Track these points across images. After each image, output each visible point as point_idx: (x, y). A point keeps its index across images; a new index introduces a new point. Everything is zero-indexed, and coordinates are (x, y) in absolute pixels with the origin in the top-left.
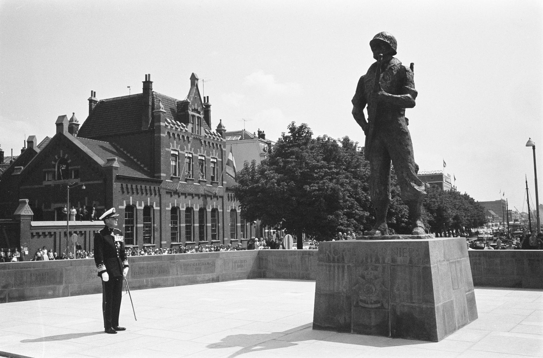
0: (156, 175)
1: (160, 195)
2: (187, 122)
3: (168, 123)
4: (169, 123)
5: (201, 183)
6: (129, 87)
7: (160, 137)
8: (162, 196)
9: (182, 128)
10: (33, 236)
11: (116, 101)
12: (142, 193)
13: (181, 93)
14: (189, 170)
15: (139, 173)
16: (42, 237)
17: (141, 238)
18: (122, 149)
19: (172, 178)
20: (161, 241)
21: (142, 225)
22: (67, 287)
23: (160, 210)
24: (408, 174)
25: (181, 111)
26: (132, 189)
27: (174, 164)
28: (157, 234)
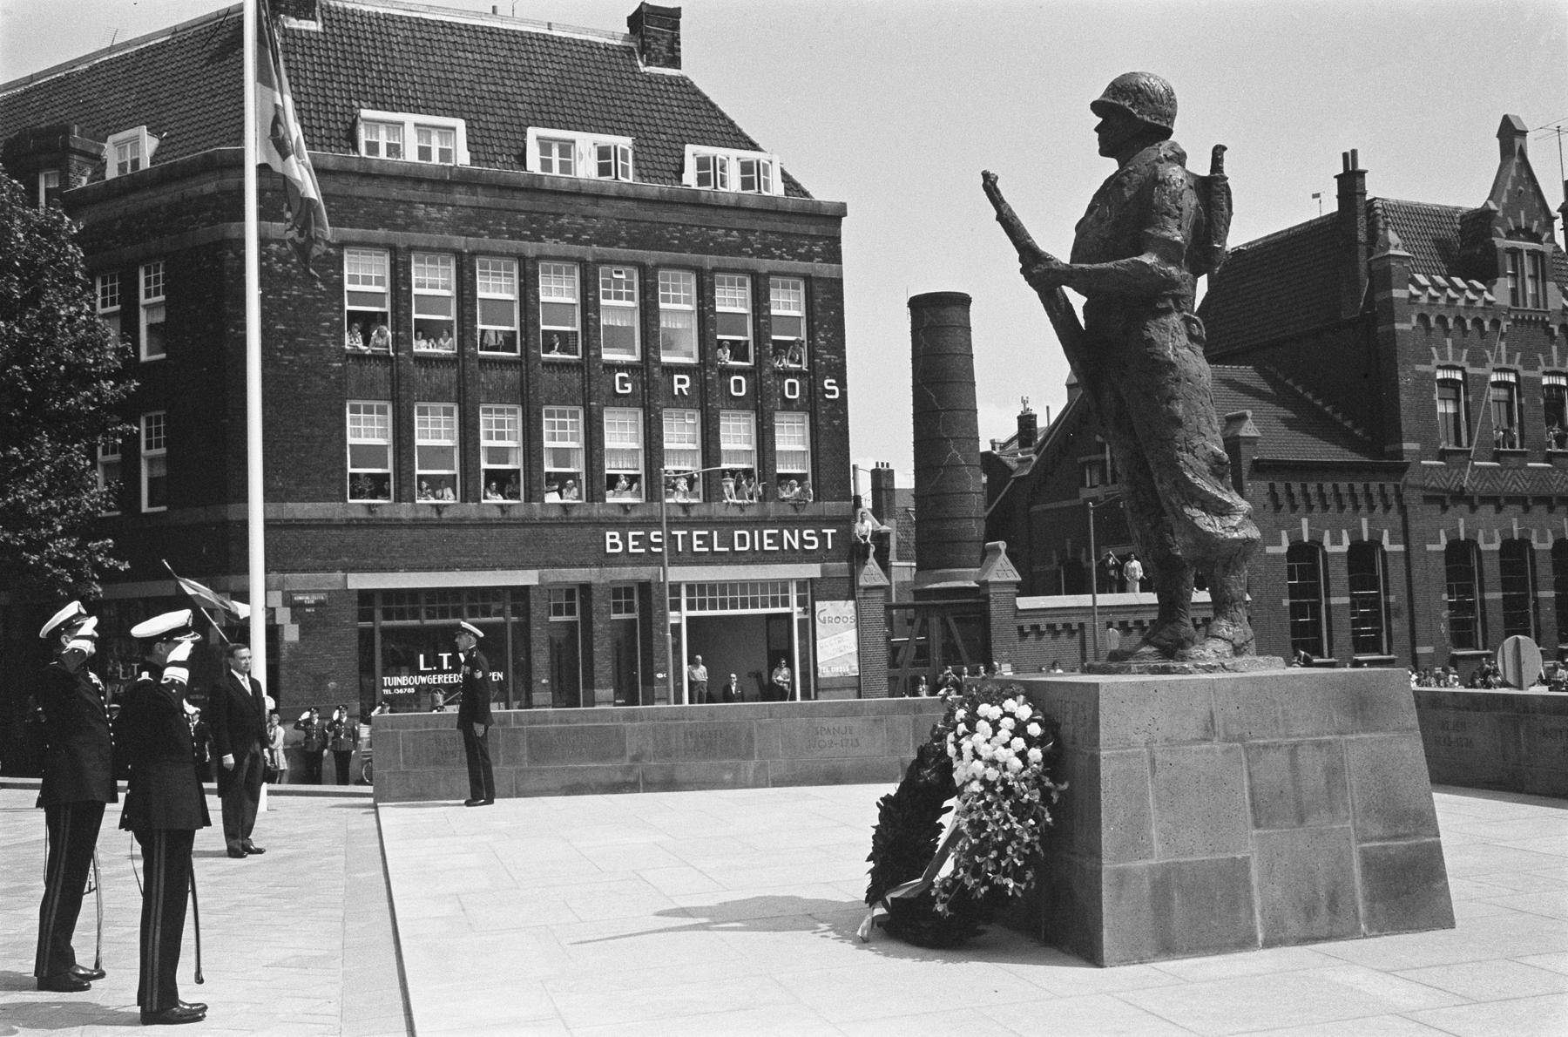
0: (1388, 448)
1: (1403, 509)
2: (1489, 275)
3: (1421, 287)
4: (1423, 288)
5: (1556, 460)
6: (1316, 196)
7: (1393, 333)
8: (1410, 510)
9: (1472, 296)
10: (1023, 634)
11: (1276, 243)
12: (1341, 507)
13: (1468, 186)
14: (1510, 421)
15: (1333, 448)
16: (1064, 635)
17: (1344, 637)
18: (1290, 382)
19: (1443, 455)
20: (1414, 644)
21: (1347, 600)
22: (763, 767)
23: (1407, 554)
24: (1175, 483)
25: (1468, 244)
26: (1306, 496)
27: (1451, 409)
28: (1399, 626)
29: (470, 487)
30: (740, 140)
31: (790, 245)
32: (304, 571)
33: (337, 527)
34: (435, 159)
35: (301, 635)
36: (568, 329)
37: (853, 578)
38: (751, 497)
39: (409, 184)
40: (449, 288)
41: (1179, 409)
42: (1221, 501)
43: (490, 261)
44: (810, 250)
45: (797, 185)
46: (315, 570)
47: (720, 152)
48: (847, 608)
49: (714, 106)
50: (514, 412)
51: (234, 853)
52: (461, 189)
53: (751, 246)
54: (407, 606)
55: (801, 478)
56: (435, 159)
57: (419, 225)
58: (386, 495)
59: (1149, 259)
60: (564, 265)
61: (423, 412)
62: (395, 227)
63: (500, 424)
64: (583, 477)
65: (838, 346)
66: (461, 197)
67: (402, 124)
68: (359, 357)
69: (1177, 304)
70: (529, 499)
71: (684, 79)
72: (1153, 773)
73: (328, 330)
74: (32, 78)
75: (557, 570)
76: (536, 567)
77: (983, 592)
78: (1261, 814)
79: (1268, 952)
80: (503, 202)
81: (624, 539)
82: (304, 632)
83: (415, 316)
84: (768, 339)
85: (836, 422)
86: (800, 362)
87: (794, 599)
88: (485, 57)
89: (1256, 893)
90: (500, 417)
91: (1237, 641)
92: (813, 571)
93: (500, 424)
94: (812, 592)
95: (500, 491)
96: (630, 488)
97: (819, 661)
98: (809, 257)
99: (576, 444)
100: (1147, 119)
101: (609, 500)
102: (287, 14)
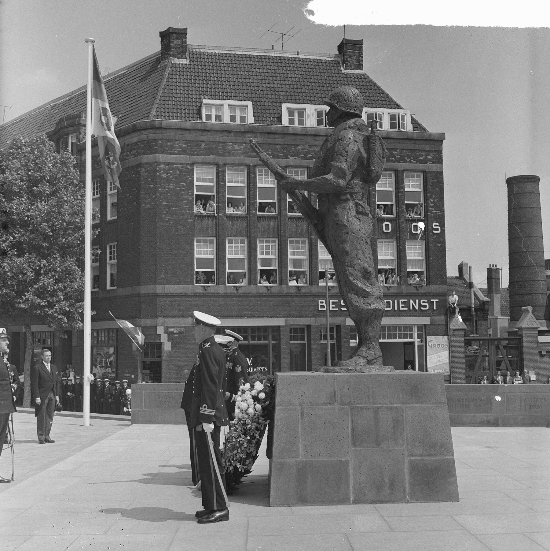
10: (542, 355)
29: (252, 278)
30: (390, 103)
31: (414, 156)
32: (174, 317)
33: (190, 297)
34: (238, 121)
35: (172, 347)
36: (241, 197)
37: (447, 325)
38: (393, 283)
39: (225, 133)
40: (243, 182)
41: (348, 247)
42: (364, 291)
43: (230, 167)
44: (427, 158)
45: (420, 125)
46: (179, 317)
47: (379, 111)
48: (443, 340)
49: (379, 88)
50: (274, 241)
51: (41, 442)
52: (249, 135)
53: (394, 157)
54: (256, 334)
55: (419, 274)
56: (238, 121)
57: (229, 153)
58: (213, 282)
59: (329, 176)
60: (300, 170)
61: (230, 242)
62: (218, 154)
63: (267, 247)
64: (308, 273)
65: (440, 205)
66: (249, 138)
67: (223, 105)
68: (201, 216)
69: (352, 197)
70: (280, 284)
71: (364, 75)
72: (302, 419)
73: (186, 204)
74: (73, 93)
75: (294, 319)
76: (284, 316)
77: (520, 333)
78: (357, 439)
79: (354, 506)
80: (269, 141)
81: (328, 304)
82: (174, 346)
83: (227, 196)
84: (403, 202)
85: (439, 245)
86: (420, 214)
87: (415, 335)
88: (265, 71)
89: (351, 478)
90: (268, 244)
91: (370, 358)
92: (426, 320)
93: (267, 247)
94: (425, 331)
95: (268, 280)
96: (332, 278)
97: (428, 366)
98: (425, 161)
99: (304, 257)
100: (344, 109)
101: (320, 284)
102: (173, 56)
